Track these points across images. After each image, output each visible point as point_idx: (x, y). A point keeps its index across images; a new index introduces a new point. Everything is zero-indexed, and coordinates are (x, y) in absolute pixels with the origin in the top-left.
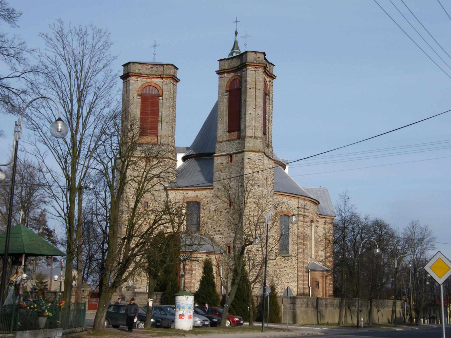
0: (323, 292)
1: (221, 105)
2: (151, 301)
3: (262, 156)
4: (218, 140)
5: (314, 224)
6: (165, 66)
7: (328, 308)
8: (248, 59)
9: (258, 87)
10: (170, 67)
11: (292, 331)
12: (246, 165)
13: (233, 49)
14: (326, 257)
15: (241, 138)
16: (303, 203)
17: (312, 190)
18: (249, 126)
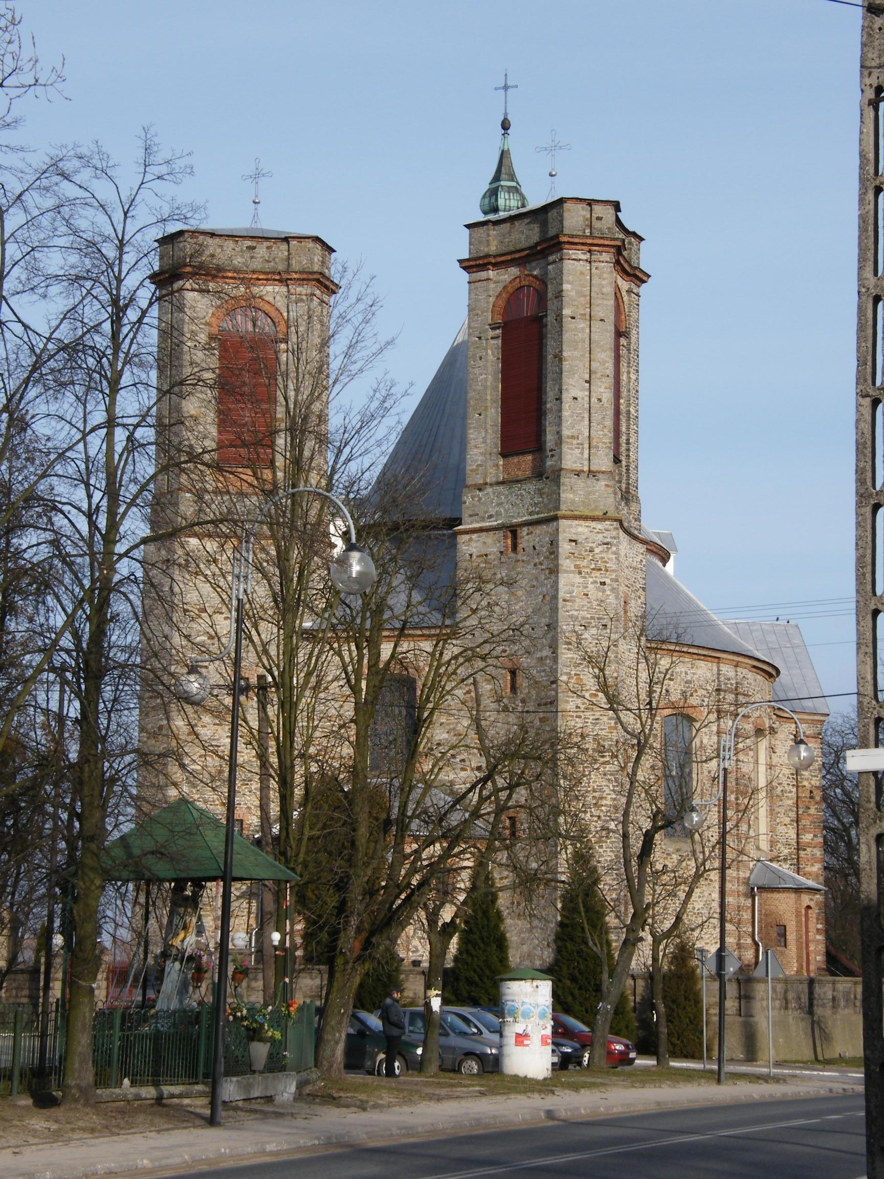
0: (799, 957)
1: (476, 371)
2: (437, 995)
3: (614, 533)
4: (470, 481)
5: (763, 744)
6: (294, 243)
7: (840, 1010)
8: (566, 223)
9: (599, 313)
10: (311, 245)
11: (785, 1081)
12: (565, 563)
13: (497, 178)
14: (799, 847)
15: (546, 475)
16: (731, 674)
17: (751, 631)
18: (573, 437)
